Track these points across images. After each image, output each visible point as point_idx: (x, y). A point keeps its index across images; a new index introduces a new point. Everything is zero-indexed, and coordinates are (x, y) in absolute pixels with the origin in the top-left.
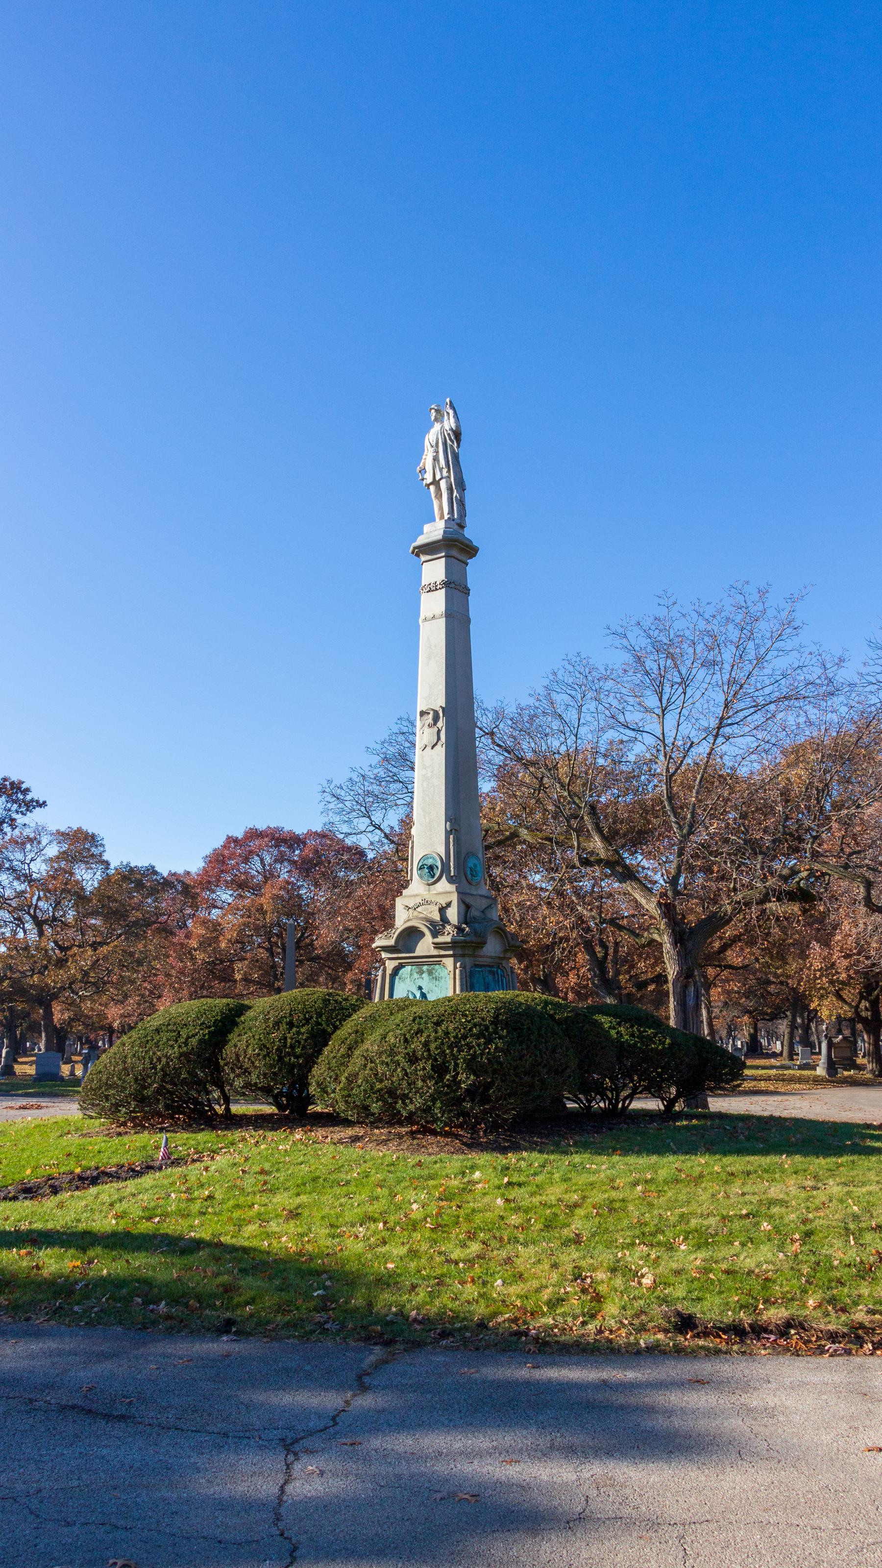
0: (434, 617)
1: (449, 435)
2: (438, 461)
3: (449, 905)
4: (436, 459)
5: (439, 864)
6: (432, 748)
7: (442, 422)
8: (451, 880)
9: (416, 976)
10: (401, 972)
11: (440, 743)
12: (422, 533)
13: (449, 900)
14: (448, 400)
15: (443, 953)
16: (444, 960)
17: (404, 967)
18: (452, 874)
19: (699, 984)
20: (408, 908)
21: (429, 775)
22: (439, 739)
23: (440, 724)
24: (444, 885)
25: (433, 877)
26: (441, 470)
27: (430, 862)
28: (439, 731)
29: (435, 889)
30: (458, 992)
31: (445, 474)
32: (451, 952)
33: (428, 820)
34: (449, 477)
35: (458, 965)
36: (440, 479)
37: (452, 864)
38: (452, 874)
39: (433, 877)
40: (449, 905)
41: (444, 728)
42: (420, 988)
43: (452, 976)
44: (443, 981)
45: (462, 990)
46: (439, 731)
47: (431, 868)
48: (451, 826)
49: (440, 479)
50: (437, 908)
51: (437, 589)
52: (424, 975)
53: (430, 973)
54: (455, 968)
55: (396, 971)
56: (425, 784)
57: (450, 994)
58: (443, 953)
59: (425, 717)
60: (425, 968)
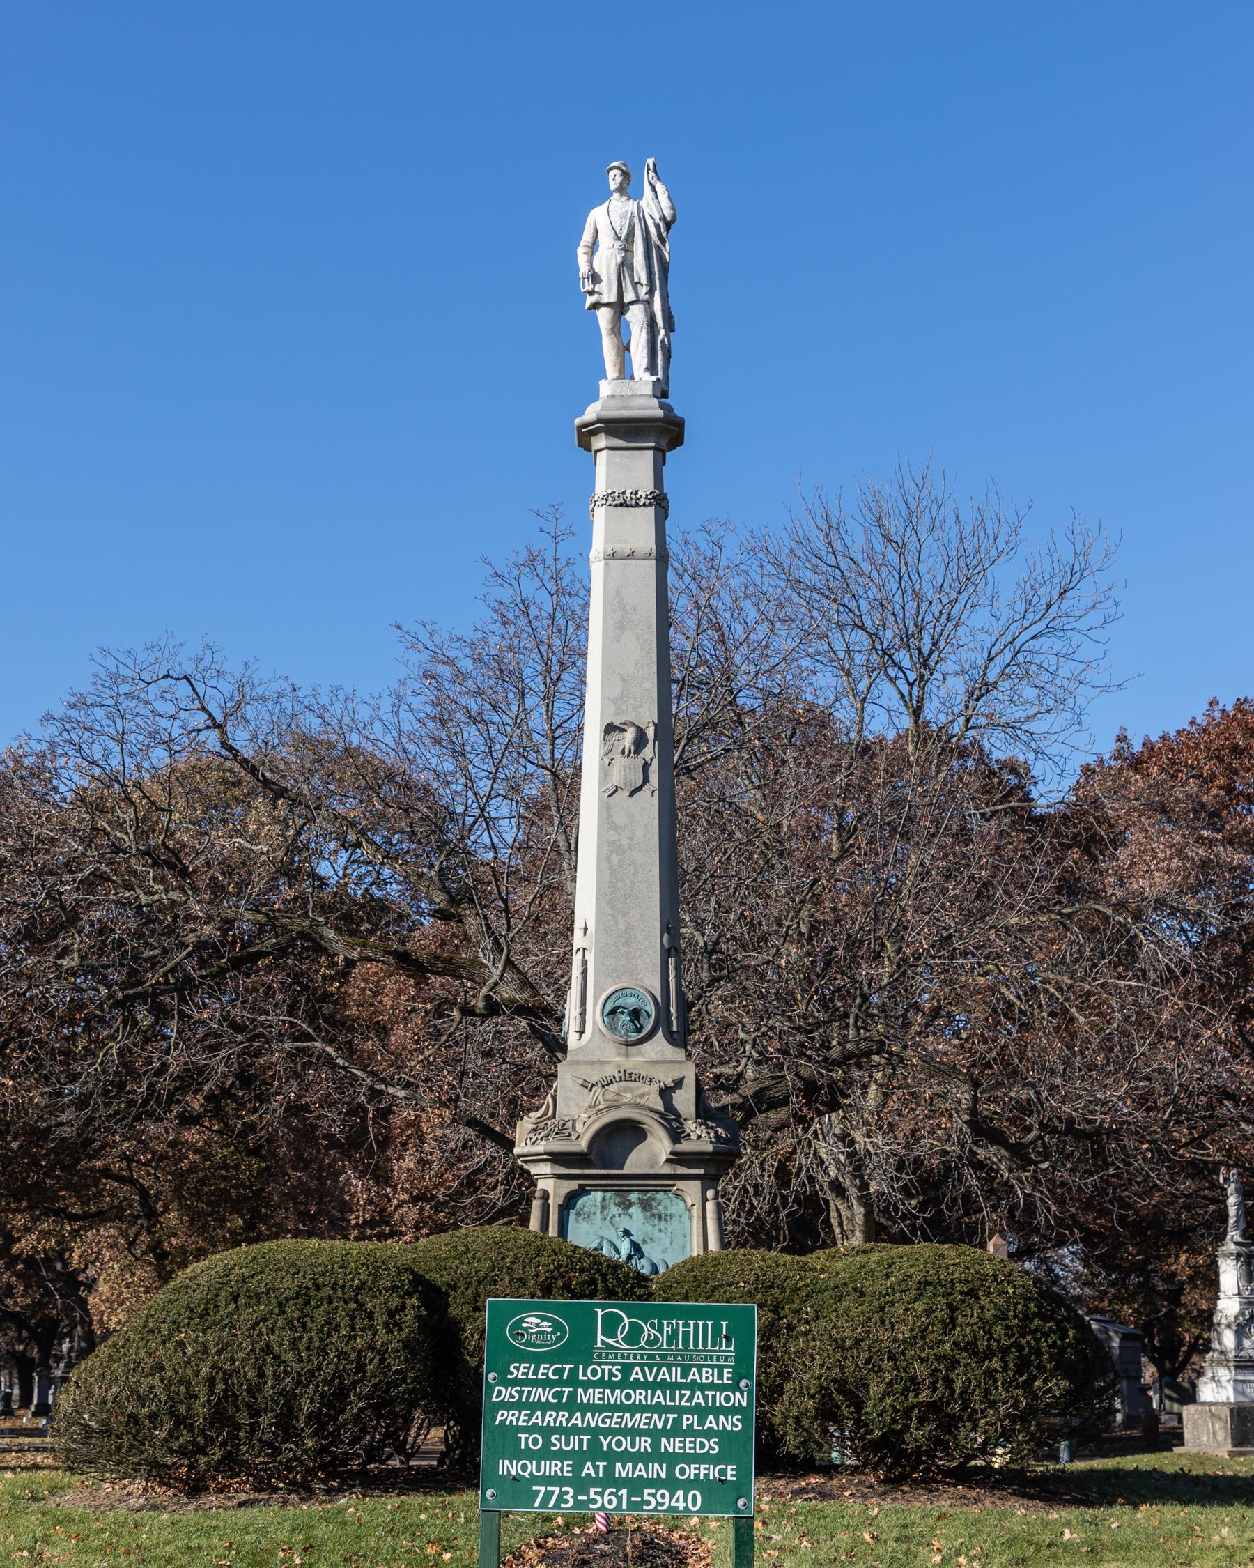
0: (632, 555)
1: (657, 227)
2: (631, 269)
3: (678, 1084)
4: (626, 265)
5: (651, 1008)
6: (632, 794)
7: (638, 196)
8: (672, 1038)
9: (615, 1210)
10: (580, 1202)
11: (647, 788)
12: (596, 398)
13: (678, 1075)
14: (650, 161)
15: (682, 1170)
16: (680, 1184)
17: (588, 1192)
18: (675, 1029)
19: (875, 1209)
20: (587, 1086)
21: (625, 842)
22: (646, 780)
23: (649, 752)
24: (659, 1047)
25: (639, 1030)
26: (635, 285)
27: (631, 1002)
28: (646, 766)
29: (639, 1054)
30: (713, 1245)
31: (643, 291)
32: (702, 1171)
33: (622, 926)
34: (649, 303)
35: (710, 1194)
36: (632, 303)
37: (673, 1010)
38: (675, 1029)
39: (639, 1030)
40: (678, 1084)
41: (655, 762)
42: (627, 1233)
43: (696, 1211)
44: (675, 1221)
45: (724, 1245)
46: (646, 766)
47: (636, 1014)
48: (670, 940)
49: (632, 303)
50: (655, 1088)
51: (637, 505)
52: (632, 1210)
53: (646, 1206)
54: (704, 1200)
55: (570, 1200)
56: (615, 859)
57: (696, 1250)
58: (682, 1170)
59: (615, 736)
60: (634, 1197)
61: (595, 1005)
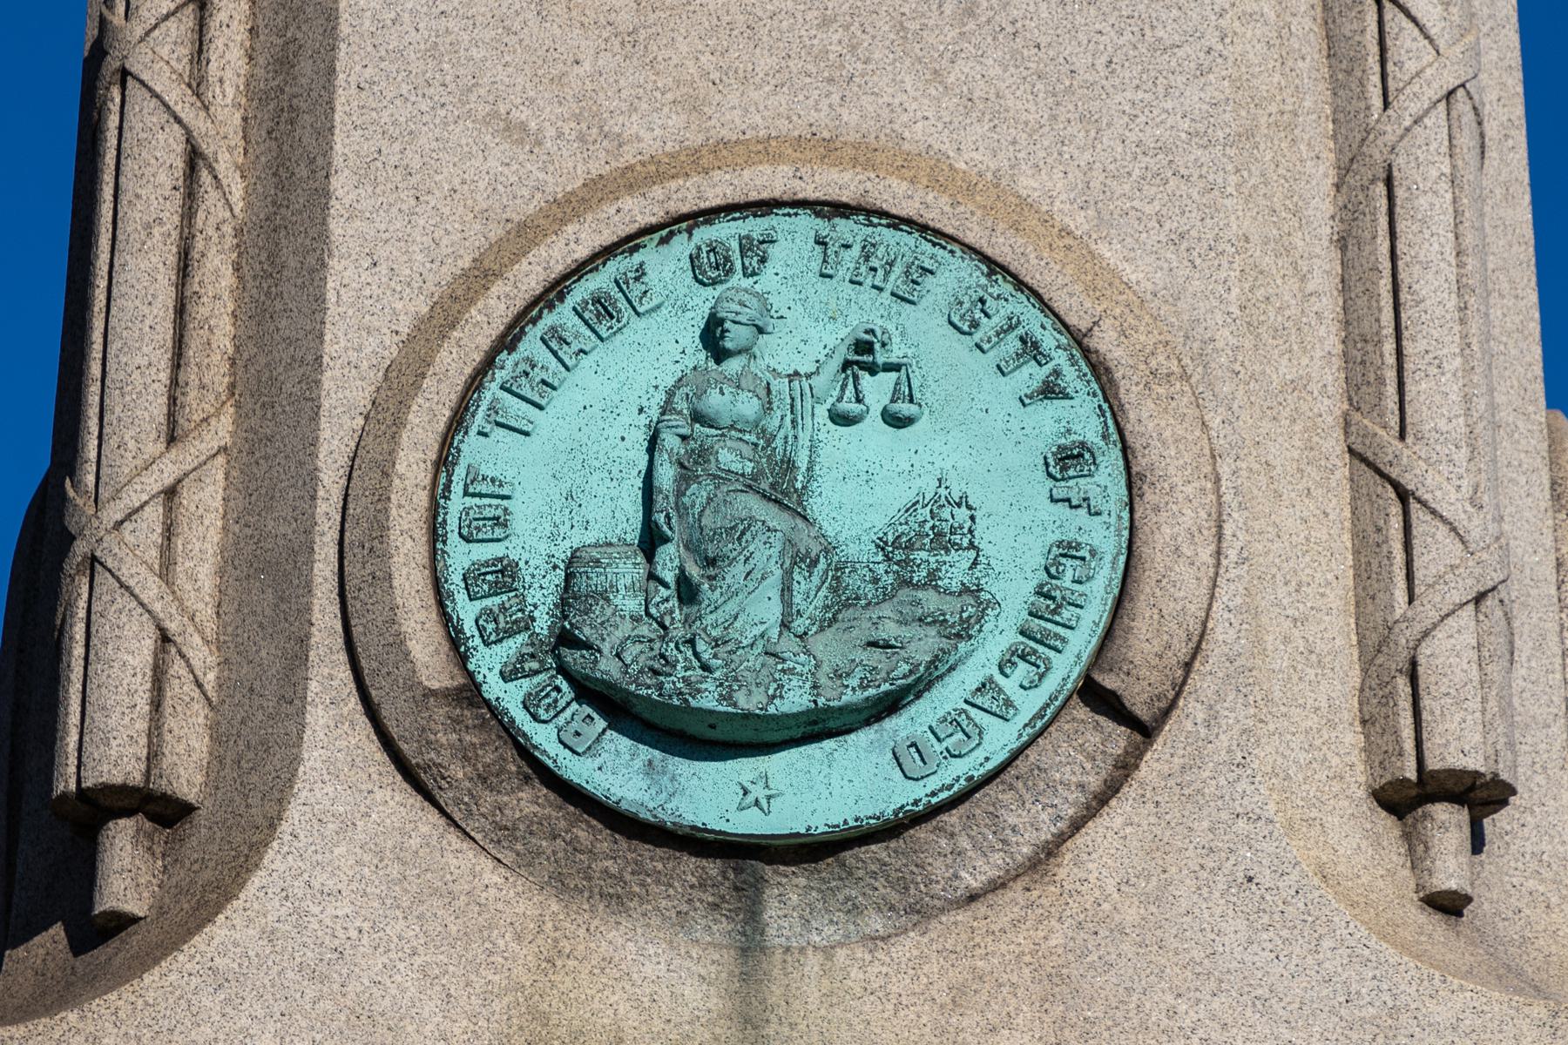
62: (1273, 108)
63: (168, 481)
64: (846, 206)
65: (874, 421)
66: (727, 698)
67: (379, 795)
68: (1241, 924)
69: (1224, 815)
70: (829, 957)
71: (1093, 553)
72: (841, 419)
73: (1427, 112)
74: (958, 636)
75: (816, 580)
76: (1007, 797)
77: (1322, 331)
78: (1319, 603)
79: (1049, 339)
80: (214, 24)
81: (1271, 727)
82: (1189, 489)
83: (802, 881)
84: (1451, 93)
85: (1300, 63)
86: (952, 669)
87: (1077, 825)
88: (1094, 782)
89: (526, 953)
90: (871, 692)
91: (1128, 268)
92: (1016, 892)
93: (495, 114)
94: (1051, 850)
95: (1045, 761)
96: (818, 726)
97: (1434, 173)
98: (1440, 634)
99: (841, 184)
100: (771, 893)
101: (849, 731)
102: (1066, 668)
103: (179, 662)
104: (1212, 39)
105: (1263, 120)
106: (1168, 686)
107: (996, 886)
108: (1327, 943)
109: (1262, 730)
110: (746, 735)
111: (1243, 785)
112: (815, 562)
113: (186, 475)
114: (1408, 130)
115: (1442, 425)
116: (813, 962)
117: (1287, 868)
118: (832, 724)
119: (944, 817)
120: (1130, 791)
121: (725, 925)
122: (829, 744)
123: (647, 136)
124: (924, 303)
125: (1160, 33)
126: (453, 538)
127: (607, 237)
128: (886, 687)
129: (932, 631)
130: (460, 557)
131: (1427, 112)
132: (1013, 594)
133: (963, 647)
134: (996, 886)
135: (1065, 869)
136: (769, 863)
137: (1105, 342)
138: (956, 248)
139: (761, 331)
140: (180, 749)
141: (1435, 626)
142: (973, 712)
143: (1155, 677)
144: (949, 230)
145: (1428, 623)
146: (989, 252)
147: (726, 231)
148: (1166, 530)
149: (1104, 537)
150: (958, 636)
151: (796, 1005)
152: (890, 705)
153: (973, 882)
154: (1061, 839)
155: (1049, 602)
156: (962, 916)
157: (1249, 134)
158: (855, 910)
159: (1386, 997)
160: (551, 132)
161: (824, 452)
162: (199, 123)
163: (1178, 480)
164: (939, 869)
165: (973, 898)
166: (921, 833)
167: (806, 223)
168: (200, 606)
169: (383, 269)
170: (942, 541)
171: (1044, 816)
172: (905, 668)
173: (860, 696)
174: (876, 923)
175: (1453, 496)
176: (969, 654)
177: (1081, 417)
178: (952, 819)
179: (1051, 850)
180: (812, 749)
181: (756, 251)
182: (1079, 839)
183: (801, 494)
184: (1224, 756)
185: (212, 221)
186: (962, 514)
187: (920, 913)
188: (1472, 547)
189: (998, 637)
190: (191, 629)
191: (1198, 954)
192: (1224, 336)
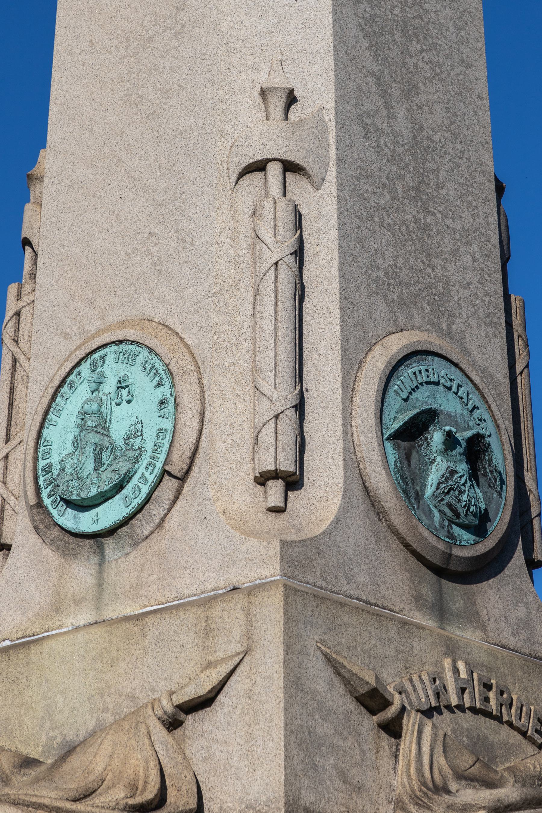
61: (349, 388)
62: (231, 281)
63: (4, 454)
64: (121, 341)
65: (124, 402)
66: (78, 495)
67: (31, 536)
68: (202, 532)
69: (201, 500)
70: (117, 562)
71: (166, 430)
72: (118, 404)
73: (267, 271)
74: (135, 463)
75: (108, 453)
76: (152, 506)
77: (246, 344)
78: (240, 427)
79: (161, 368)
80: (21, 319)
81: (216, 470)
82: (191, 405)
83: (111, 541)
84: (276, 264)
85: (242, 264)
86: (135, 473)
87: (169, 511)
88: (172, 497)
89: (56, 575)
90: (111, 485)
91: (189, 340)
92: (156, 534)
93: (62, 332)
94: (163, 519)
95: (160, 494)
96: (104, 498)
97: (269, 289)
98: (263, 431)
99: (119, 335)
100: (106, 546)
101: (114, 496)
102: (159, 466)
103: (8, 505)
104: (210, 266)
105: (226, 286)
106: (185, 465)
107: (152, 533)
108: (221, 533)
109: (211, 472)
110: (91, 503)
111: (206, 490)
112: (107, 448)
113: (10, 451)
114: (262, 278)
115: (267, 366)
116: (114, 563)
117: (213, 512)
118: (109, 495)
119: (138, 516)
120: (181, 498)
121: (97, 558)
122: (110, 501)
123: (92, 329)
124: (136, 365)
125: (200, 267)
126: (40, 459)
127: (73, 364)
128: (114, 483)
129: (128, 463)
130: (42, 464)
131: (267, 271)
132: (149, 446)
133: (137, 466)
134: (152, 533)
135: (166, 525)
136: (103, 538)
137: (172, 367)
138: (143, 346)
139: (101, 383)
140: (8, 530)
141: (261, 429)
142: (140, 484)
143: (180, 463)
144: (142, 342)
145: (259, 428)
146: (149, 346)
147: (97, 355)
148: (182, 419)
149: (169, 425)
150: (135, 463)
151: (110, 578)
152: (119, 487)
153: (146, 533)
154: (166, 515)
155: (157, 447)
156: (144, 544)
157: (220, 291)
158: (123, 547)
159: (232, 546)
160: (74, 334)
161: (114, 415)
162: (15, 349)
163: (187, 403)
164: (139, 531)
165: (147, 537)
166: (133, 521)
167: (114, 348)
168: (15, 488)
169: (38, 384)
170: (135, 435)
171: (161, 510)
172: (117, 476)
173: (109, 486)
174: (128, 550)
175: (268, 387)
176: (139, 468)
177: (165, 391)
178: (139, 516)
179: (163, 519)
180: (107, 503)
181: (103, 359)
182: (170, 515)
183: (108, 430)
184: (202, 482)
185: (20, 376)
186: (140, 425)
187: (136, 544)
188: (274, 401)
189: (146, 459)
190: (10, 495)
191: (193, 543)
192: (209, 355)
